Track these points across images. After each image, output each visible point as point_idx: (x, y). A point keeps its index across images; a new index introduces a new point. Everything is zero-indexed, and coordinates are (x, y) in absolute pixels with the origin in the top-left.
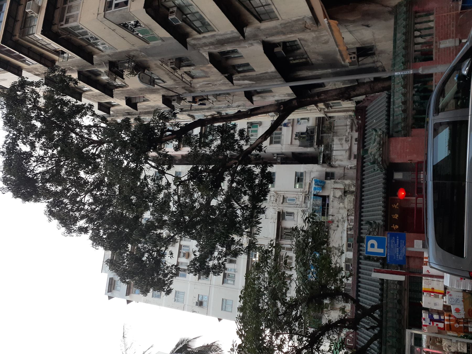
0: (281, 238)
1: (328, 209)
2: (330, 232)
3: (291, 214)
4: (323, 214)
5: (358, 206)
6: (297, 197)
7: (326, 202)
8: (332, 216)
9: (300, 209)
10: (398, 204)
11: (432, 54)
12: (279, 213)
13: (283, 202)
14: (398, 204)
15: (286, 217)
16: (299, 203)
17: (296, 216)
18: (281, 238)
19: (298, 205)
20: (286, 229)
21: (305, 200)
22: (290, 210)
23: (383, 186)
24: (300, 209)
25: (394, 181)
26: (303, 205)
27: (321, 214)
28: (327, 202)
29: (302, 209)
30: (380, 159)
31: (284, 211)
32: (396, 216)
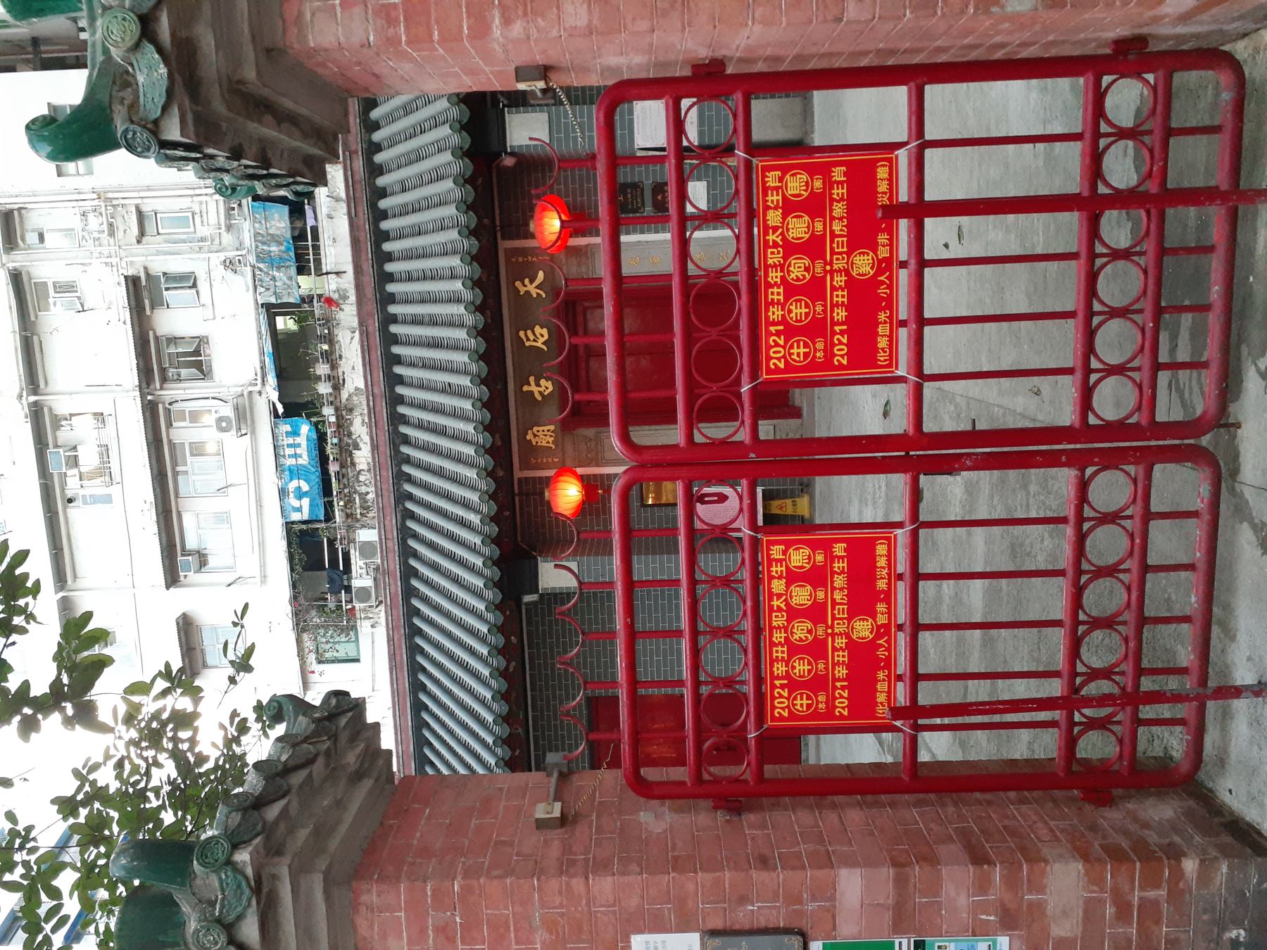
0: (164, 379)
1: (316, 248)
2: (340, 338)
3: (188, 281)
4: (302, 270)
5: (369, 291)
6: (196, 208)
7: (305, 224)
8: (337, 273)
9: (217, 259)
10: (541, 275)
11: (605, 392)
12: (133, 283)
13: (142, 233)
14: (541, 275)
15: (165, 293)
16: (203, 231)
17: (203, 285)
18: (164, 379)
19: (202, 240)
20: (173, 340)
21: (229, 216)
22: (176, 265)
23: (458, 194)
24: (217, 259)
25: (509, 162)
26: (227, 238)
27: (293, 271)
28: (310, 222)
29: (222, 256)
30: (151, 75)
31: (152, 272)
32: (539, 337)
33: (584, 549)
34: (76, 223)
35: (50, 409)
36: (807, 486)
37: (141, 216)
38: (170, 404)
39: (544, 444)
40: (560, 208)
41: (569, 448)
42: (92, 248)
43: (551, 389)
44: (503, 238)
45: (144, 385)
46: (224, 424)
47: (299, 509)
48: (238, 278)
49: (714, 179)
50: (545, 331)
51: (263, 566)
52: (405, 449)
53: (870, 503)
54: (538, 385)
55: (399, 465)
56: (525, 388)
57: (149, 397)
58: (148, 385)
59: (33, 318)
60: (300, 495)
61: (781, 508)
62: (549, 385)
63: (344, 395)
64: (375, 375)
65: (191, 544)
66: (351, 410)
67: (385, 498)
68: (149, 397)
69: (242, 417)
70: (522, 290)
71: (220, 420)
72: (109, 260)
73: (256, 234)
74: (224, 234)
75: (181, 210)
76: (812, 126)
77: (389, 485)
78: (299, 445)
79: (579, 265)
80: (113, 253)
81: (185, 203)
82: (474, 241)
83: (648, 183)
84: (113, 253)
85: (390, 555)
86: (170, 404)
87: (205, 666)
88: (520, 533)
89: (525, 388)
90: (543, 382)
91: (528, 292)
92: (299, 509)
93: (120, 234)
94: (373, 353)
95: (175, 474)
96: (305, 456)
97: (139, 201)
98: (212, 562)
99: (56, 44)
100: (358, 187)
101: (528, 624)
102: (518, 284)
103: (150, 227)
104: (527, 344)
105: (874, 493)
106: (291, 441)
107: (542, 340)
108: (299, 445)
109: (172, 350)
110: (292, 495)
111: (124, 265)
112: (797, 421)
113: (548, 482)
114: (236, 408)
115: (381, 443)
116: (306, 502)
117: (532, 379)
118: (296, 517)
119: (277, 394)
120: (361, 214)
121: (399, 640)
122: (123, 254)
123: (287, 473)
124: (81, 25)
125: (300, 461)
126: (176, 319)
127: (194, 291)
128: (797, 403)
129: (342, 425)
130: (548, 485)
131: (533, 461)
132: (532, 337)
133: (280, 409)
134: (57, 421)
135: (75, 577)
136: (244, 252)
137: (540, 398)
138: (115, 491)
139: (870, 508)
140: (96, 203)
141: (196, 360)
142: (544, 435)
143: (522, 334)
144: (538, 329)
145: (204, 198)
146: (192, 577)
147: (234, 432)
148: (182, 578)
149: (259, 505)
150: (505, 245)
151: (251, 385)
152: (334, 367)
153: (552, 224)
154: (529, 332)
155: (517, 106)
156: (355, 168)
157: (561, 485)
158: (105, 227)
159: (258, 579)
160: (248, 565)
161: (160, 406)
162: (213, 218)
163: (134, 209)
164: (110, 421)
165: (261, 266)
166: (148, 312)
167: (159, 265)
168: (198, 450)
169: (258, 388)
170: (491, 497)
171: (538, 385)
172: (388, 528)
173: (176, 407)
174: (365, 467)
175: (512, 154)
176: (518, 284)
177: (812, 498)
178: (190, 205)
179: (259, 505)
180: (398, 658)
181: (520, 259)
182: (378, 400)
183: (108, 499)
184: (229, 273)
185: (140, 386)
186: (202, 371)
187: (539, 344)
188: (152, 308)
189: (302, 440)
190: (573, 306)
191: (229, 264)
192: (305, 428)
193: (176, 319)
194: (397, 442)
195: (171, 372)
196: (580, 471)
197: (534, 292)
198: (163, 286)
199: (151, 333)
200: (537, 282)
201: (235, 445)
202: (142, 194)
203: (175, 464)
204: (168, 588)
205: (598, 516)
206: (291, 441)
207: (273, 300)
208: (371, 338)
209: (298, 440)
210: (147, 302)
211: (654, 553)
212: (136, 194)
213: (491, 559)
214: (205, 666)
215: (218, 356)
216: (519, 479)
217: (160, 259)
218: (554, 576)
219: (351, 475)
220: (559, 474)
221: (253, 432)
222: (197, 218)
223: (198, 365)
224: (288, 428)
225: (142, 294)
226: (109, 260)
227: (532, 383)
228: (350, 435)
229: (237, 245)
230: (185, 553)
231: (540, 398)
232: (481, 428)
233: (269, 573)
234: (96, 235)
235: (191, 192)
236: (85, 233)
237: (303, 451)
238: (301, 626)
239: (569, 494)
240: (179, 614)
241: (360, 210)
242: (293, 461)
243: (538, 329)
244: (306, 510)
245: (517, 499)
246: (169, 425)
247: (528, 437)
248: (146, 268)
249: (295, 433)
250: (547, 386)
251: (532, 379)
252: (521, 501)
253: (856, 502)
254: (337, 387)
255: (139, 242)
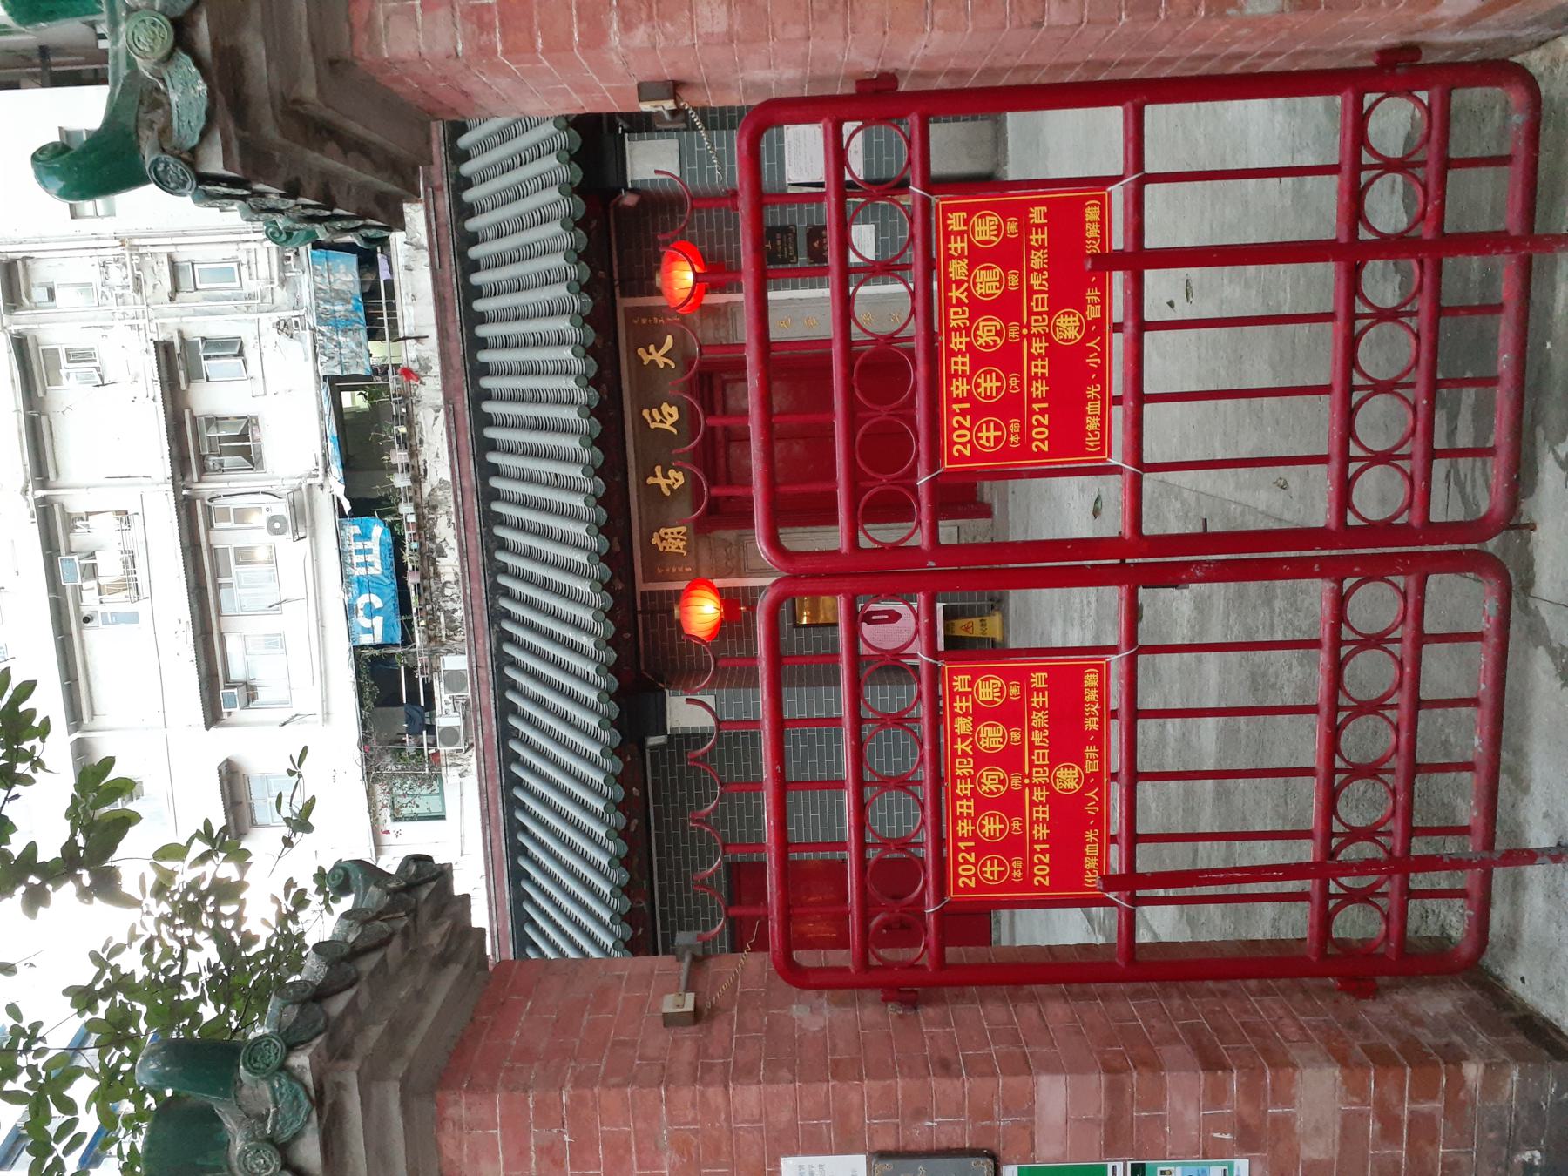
0: (203, 470)
1: (392, 307)
2: (421, 418)
3: (233, 348)
4: (374, 334)
5: (457, 361)
6: (243, 258)
7: (378, 277)
8: (417, 338)
9: (268, 320)
10: (669, 340)
11: (749, 485)
12: (164, 350)
13: (176, 288)
14: (669, 340)
15: (204, 363)
16: (251, 286)
17: (251, 353)
18: (203, 470)
19: (250, 297)
20: (214, 421)
21: (283, 268)
22: (218, 328)
23: (566, 240)
24: (268, 320)
25: (630, 200)
26: (281, 295)
27: (363, 335)
28: (384, 275)
29: (275, 317)
30: (187, 93)
31: (188, 337)
32: (667, 417)
33: (723, 680)
34: (95, 276)
35: (62, 507)
36: (999, 601)
37: (174, 267)
38: (211, 500)
39: (673, 549)
40: (693, 257)
41: (704, 555)
42: (114, 307)
43: (682, 481)
44: (623, 295)
45: (179, 477)
46: (277, 525)
47: (371, 631)
48: (294, 344)
49: (884, 222)
50: (674, 410)
51: (325, 700)
52: (501, 556)
53: (1076, 622)
54: (666, 477)
55: (494, 576)
56: (650, 481)
57: (185, 492)
58: (183, 476)
59: (40, 394)
60: (371, 612)
61: (967, 629)
62: (680, 476)
63: (426, 489)
64: (464, 464)
65: (237, 673)
66: (434, 508)
67: (477, 617)
68: (185, 492)
69: (300, 516)
70: (646, 359)
71: (272, 520)
72: (134, 322)
73: (317, 290)
74: (278, 290)
75: (224, 260)
76: (1005, 156)
77: (481, 601)
78: (370, 551)
79: (717, 328)
80: (140, 313)
81: (229, 251)
82: (587, 299)
83: (802, 227)
84: (140, 313)
85: (483, 687)
86: (211, 500)
87: (254, 824)
88: (643, 660)
89: (650, 481)
90: (672, 473)
91: (653, 362)
92: (371, 631)
93: (148, 290)
94: (461, 437)
95: (217, 587)
96: (378, 565)
97: (172, 249)
98: (262, 695)
99: (70, 55)
100: (443, 231)
101: (654, 772)
102: (641, 351)
103: (186, 281)
104: (653, 426)
105: (1082, 611)
106: (360, 546)
107: (671, 421)
108: (370, 551)
109: (213, 433)
110: (361, 613)
111: (153, 328)
112: (987, 522)
113: (678, 597)
114: (293, 505)
115: (472, 549)
116: (378, 621)
117: (658, 469)
118: (366, 639)
119: (343, 487)
120: (446, 265)
121: (494, 792)
122: (152, 314)
123: (355, 585)
124: (100, 31)
125: (372, 571)
126: (218, 395)
127: (240, 360)
128: (987, 499)
129: (423, 527)
130: (678, 601)
131: (660, 571)
132: (658, 418)
133: (347, 507)
134: (70, 522)
135: (93, 714)
136: (302, 312)
137: (668, 493)
138: (142, 607)
139: (1077, 629)
140: (119, 251)
141: (243, 445)
142: (673, 539)
143: (646, 413)
144: (665, 408)
145: (252, 246)
146: (238, 714)
147: (289, 534)
148: (225, 716)
149: (321, 625)
150: (625, 303)
151: (310, 476)
152: (413, 454)
153: (684, 277)
154: (655, 411)
155: (640, 131)
156: (440, 208)
157: (694, 600)
158: (130, 281)
159: (319, 717)
160: (308, 700)
161: (198, 502)
162: (263, 270)
163: (165, 259)
164: (136, 522)
165: (323, 329)
166: (183, 387)
167: (197, 328)
168: (245, 557)
169: (320, 480)
170: (607, 615)
171: (666, 477)
172: (480, 653)
173: (217, 504)
174: (451, 578)
175: (634, 191)
176: (641, 351)
177: (1005, 617)
178: (235, 254)
179: (321, 625)
180: (493, 815)
181: (644, 321)
182: (468, 495)
183: (133, 618)
184: (284, 338)
185: (173, 478)
186: (250, 460)
187: (667, 426)
188: (189, 381)
189: (374, 545)
190: (709, 379)
191: (284, 327)
192: (378, 530)
193: (218, 395)
194: (492, 547)
195: (212, 461)
196: (717, 583)
197: (661, 361)
198: (202, 355)
199: (187, 412)
200: (664, 350)
201: (291, 551)
202: (176, 240)
203: (216, 574)
204: (207, 728)
205: (740, 638)
206: (360, 546)
207: (338, 372)
208: (460, 418)
209: (369, 545)
210: (182, 374)
211: (810, 685)
212: (168, 241)
213: (607, 691)
214: (254, 824)
215: (270, 441)
216: (643, 594)
217: (198, 321)
218: (686, 713)
219: (434, 588)
220: (692, 587)
221: (314, 535)
222: (244, 269)
223: (246, 452)
224: (356, 529)
225: (176, 364)
226: (134, 322)
227: (659, 474)
228: (433, 538)
229: (293, 303)
230: (229, 684)
231: (668, 493)
232: (595, 530)
233: (333, 709)
234: (119, 291)
235: (236, 238)
236: (105, 289)
237: (375, 558)
238: (372, 775)
239: (704, 612)
240: (222, 760)
241: (445, 259)
242: (362, 571)
243: (665, 408)
244: (379, 631)
245: (640, 617)
246: (210, 526)
247: (654, 541)
248: (180, 332)
249: (365, 536)
250: (677, 478)
251: (658, 469)
252: (644, 620)
253: (1059, 621)
254: (417, 479)
255: (171, 299)
